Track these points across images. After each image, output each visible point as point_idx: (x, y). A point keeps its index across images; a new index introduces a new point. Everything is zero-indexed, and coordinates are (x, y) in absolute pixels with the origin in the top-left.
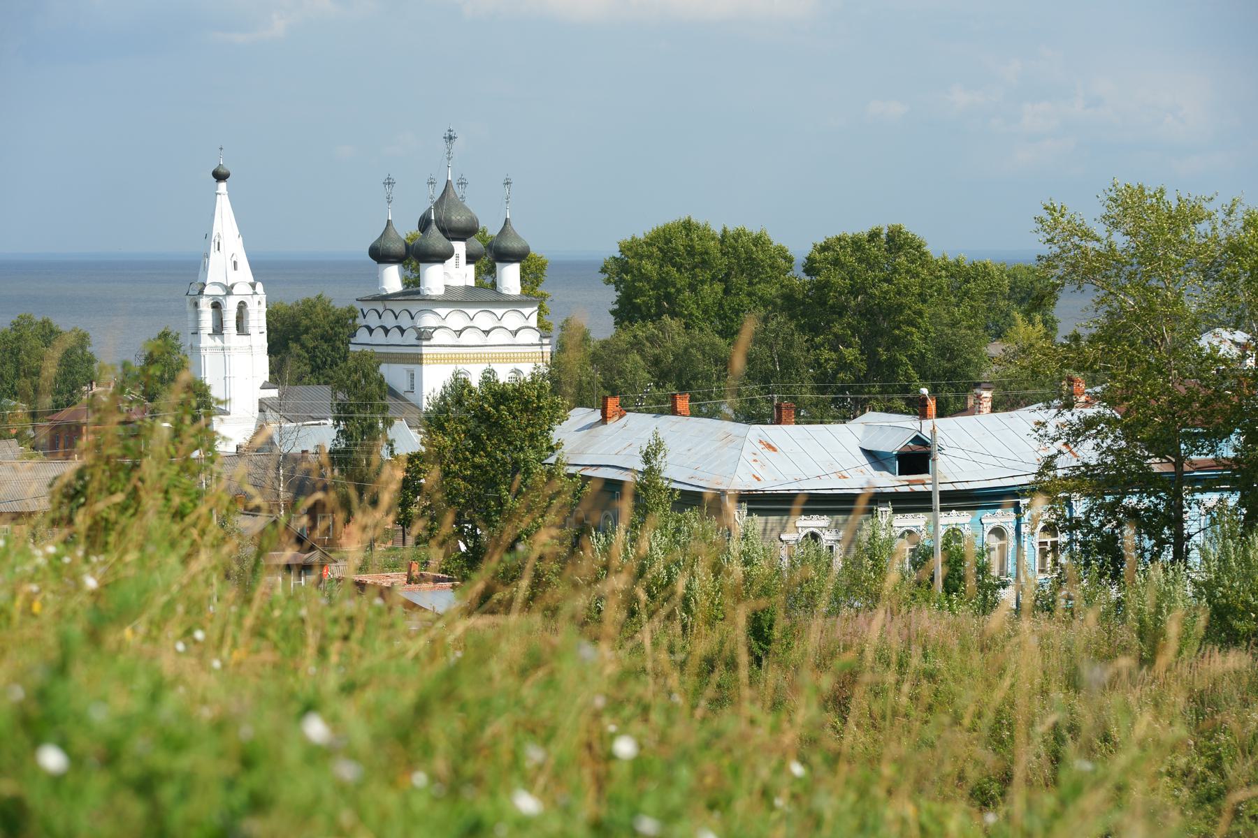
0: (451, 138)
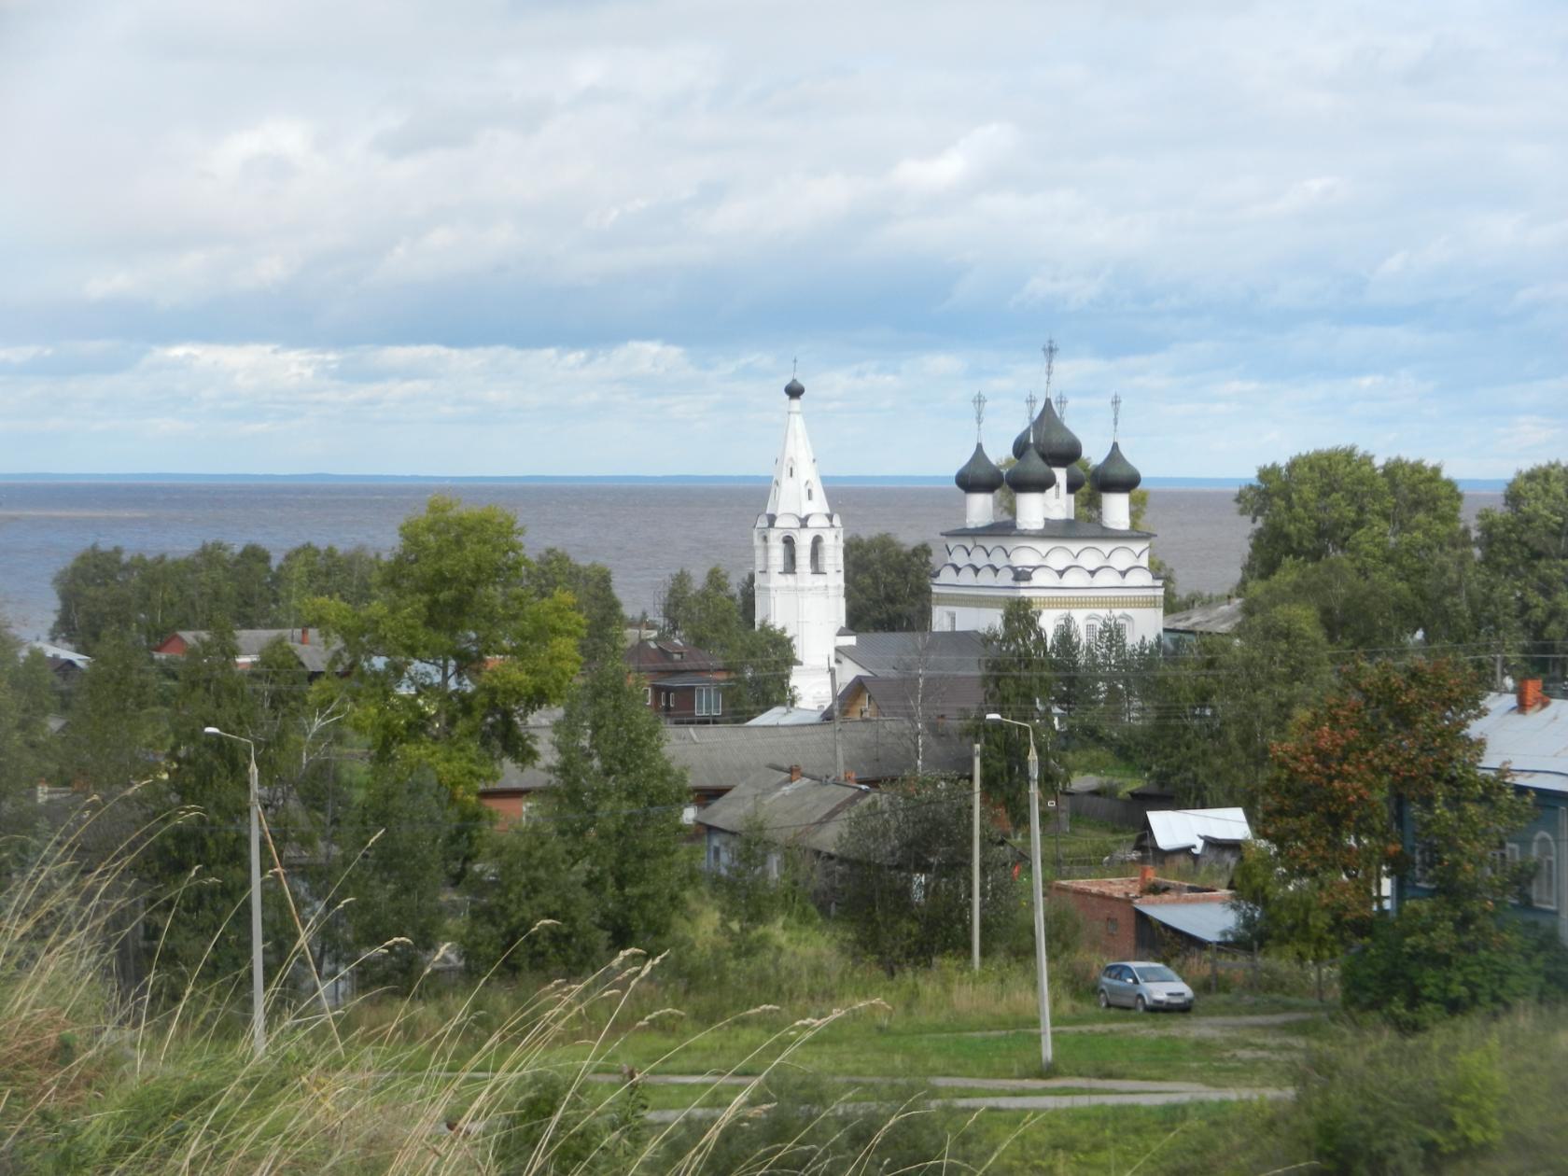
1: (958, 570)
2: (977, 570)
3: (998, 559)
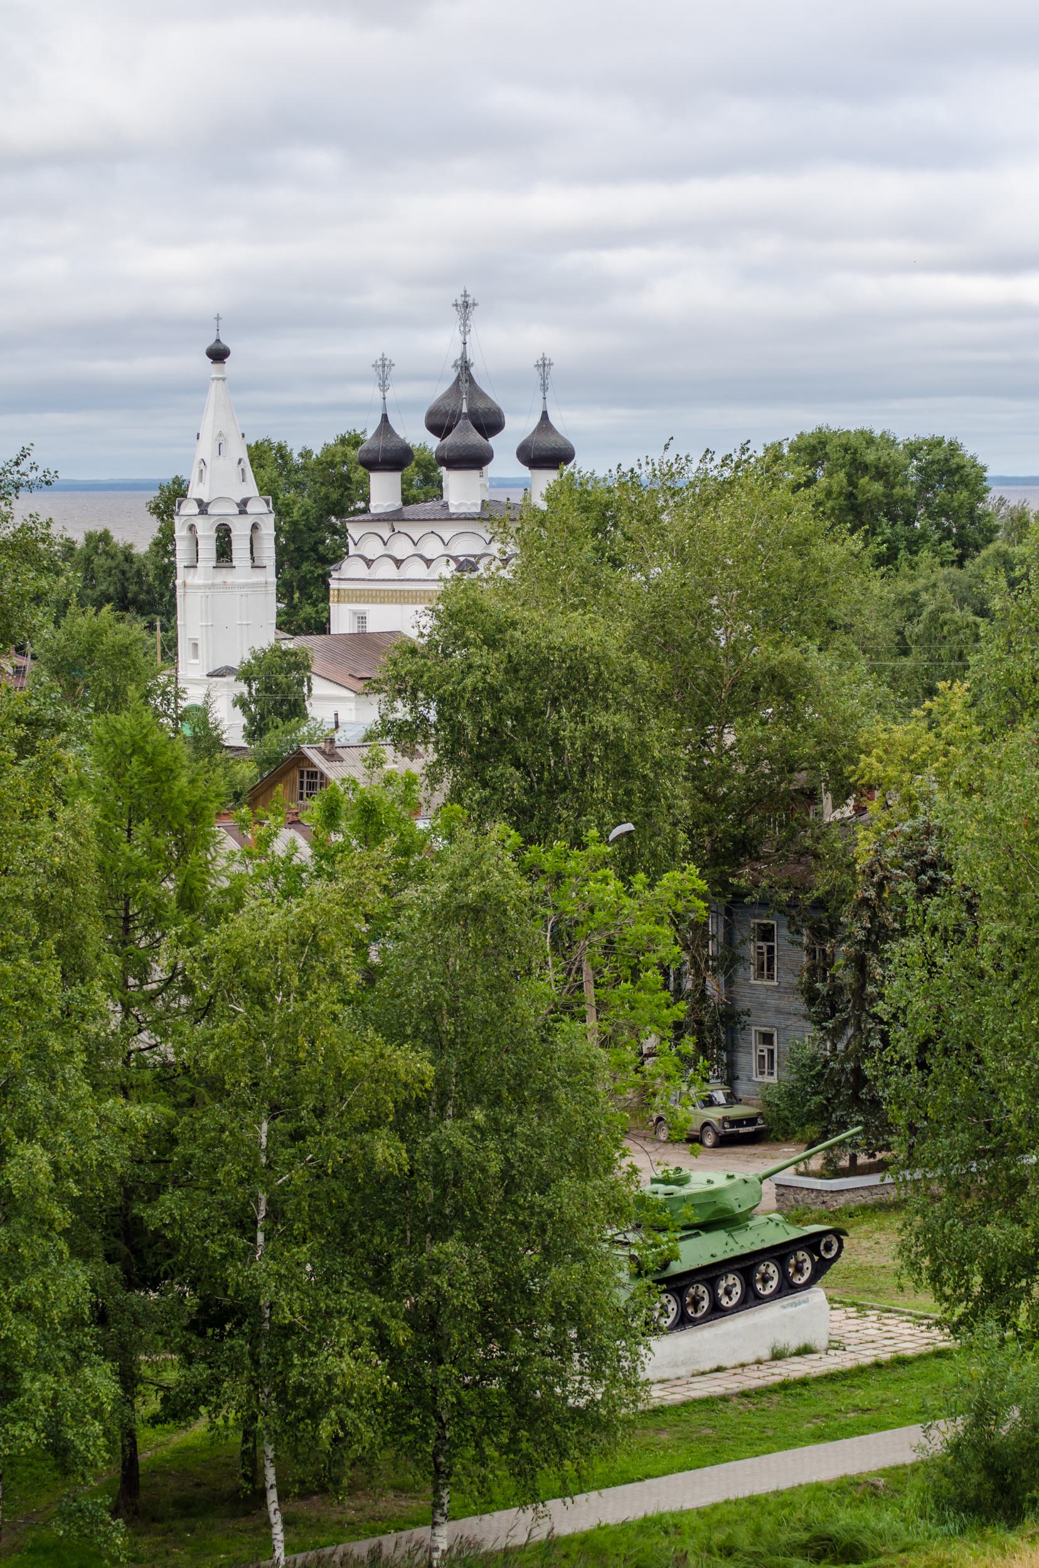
0: (466, 305)
1: (369, 563)
2: (398, 563)
3: (432, 548)
